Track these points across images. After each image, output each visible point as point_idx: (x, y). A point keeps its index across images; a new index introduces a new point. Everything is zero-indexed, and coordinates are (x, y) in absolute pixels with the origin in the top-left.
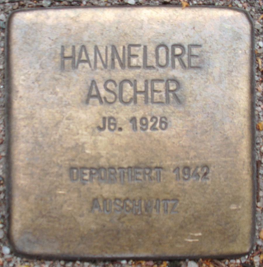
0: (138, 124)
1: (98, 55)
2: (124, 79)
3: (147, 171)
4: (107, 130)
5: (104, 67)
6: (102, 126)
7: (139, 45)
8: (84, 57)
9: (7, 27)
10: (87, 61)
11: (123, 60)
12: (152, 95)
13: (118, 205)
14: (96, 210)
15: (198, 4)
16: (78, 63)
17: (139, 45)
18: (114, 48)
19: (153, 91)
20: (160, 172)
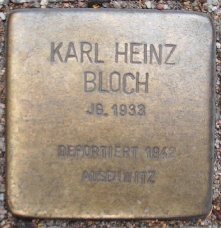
0: (119, 111)
3: (126, 149)
5: (158, 62)
6: (90, 111)
7: (139, 44)
9: (7, 22)
10: (75, 56)
11: (160, 57)
12: (131, 57)
17: (139, 44)
20: (136, 150)
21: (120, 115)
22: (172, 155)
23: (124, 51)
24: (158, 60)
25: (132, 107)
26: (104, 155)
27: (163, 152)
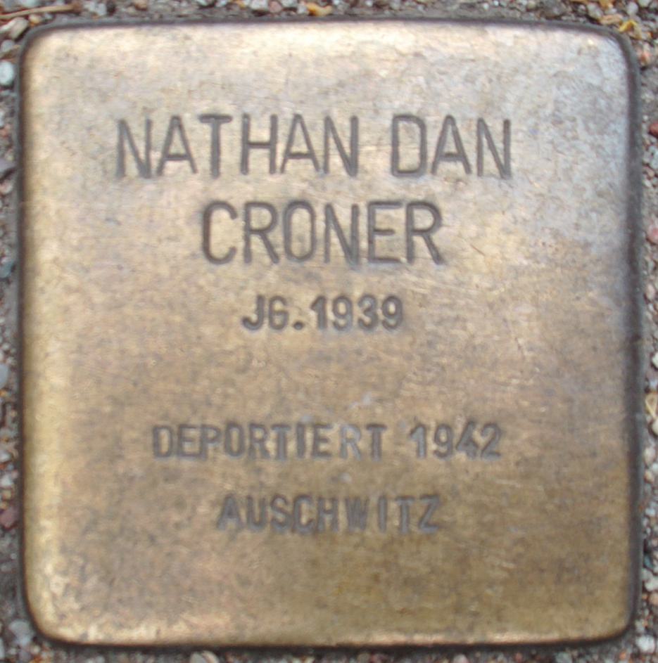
1: (331, 141)
2: (429, 200)
4: (380, 328)
6: (254, 318)
8: (177, 147)
10: (460, 156)
13: (281, 510)
14: (231, 524)
15: (350, 15)
16: (285, 161)
18: (123, 126)
19: (374, 231)
21: (247, 327)
22: (489, 449)
23: (265, 136)
24: (348, 161)
25: (367, 304)
26: (422, 450)
27: (465, 440)
